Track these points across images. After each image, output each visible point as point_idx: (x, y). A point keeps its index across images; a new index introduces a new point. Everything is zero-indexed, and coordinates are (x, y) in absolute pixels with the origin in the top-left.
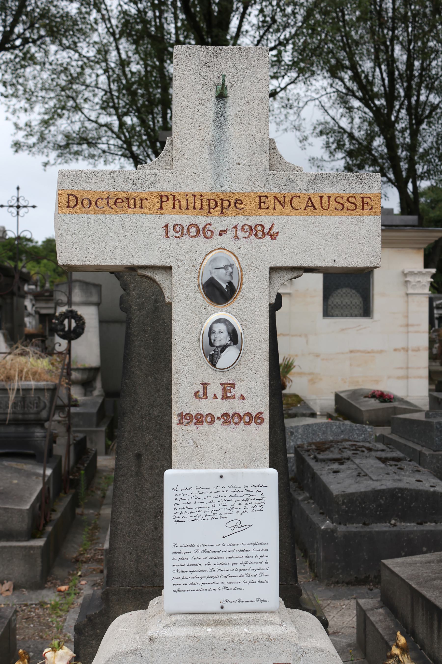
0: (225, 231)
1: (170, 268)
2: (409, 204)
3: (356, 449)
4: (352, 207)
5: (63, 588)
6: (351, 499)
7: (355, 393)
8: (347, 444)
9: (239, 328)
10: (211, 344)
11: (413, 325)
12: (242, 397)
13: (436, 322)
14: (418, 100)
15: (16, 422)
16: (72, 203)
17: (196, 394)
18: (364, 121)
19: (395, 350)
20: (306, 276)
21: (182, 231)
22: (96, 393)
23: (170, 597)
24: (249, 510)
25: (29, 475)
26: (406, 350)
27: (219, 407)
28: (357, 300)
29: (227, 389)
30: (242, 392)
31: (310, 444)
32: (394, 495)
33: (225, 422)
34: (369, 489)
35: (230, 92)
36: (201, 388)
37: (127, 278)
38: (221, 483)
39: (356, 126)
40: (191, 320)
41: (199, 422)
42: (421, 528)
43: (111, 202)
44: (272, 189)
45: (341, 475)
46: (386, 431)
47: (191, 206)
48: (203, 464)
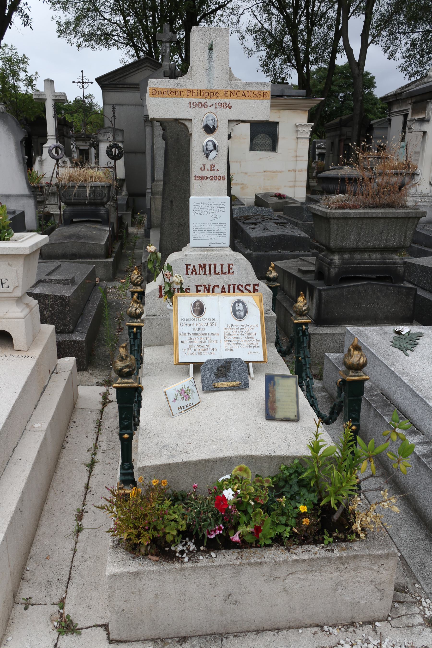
0: (212, 105)
1: (191, 120)
2: (304, 80)
3: (264, 219)
4: (259, 96)
5: (123, 281)
6: (259, 239)
7: (266, 195)
8: (259, 217)
9: (217, 144)
10: (207, 150)
11: (299, 156)
12: (218, 170)
13: (317, 157)
14: (313, 10)
15: (90, 204)
16: (154, 93)
17: (201, 169)
18: (279, 23)
19: (289, 171)
20: (242, 124)
21: (196, 105)
22: (124, 193)
23: (193, 242)
24: (220, 211)
25: (100, 230)
26: (295, 171)
27: (209, 174)
28: (269, 141)
29: (212, 166)
30: (217, 168)
31: (241, 217)
32: (280, 238)
33: (211, 179)
34: (269, 235)
35: (214, 47)
36: (203, 166)
37: (165, 124)
38: (210, 201)
39: (274, 27)
40: (199, 140)
41: (202, 179)
42: (292, 253)
43: (169, 93)
44: (229, 88)
45: (255, 230)
46: (281, 214)
47: (199, 95)
48: (204, 194)
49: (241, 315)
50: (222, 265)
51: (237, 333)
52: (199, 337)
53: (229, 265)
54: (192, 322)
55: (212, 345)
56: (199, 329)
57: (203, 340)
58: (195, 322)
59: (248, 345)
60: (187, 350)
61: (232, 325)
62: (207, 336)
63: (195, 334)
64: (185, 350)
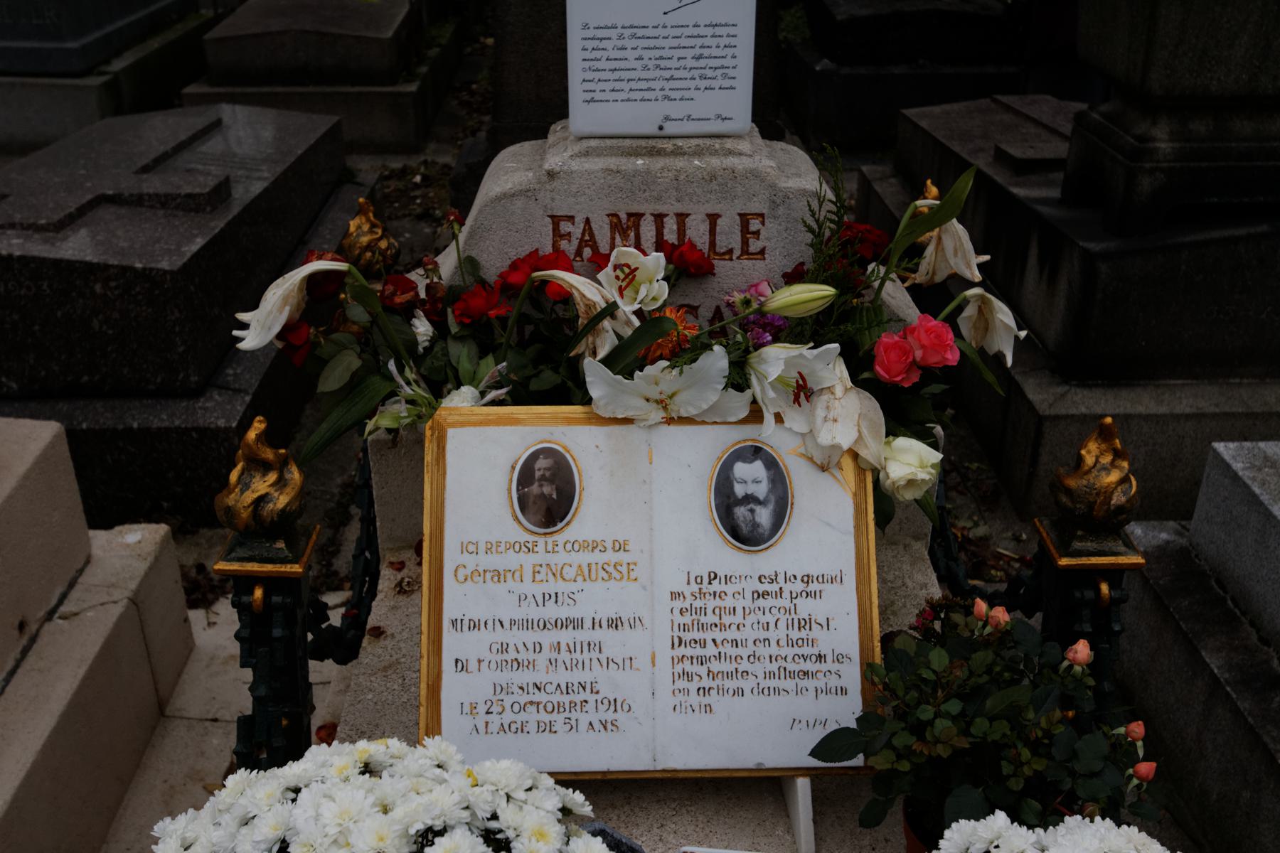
49: (755, 525)
50: (713, 218)
51: (738, 618)
52: (548, 638)
53: (744, 218)
54: (511, 560)
55: (610, 683)
56: (546, 597)
57: (564, 655)
58: (528, 560)
59: (789, 684)
60: (482, 709)
61: (713, 577)
62: (584, 635)
63: (527, 624)
64: (474, 707)
